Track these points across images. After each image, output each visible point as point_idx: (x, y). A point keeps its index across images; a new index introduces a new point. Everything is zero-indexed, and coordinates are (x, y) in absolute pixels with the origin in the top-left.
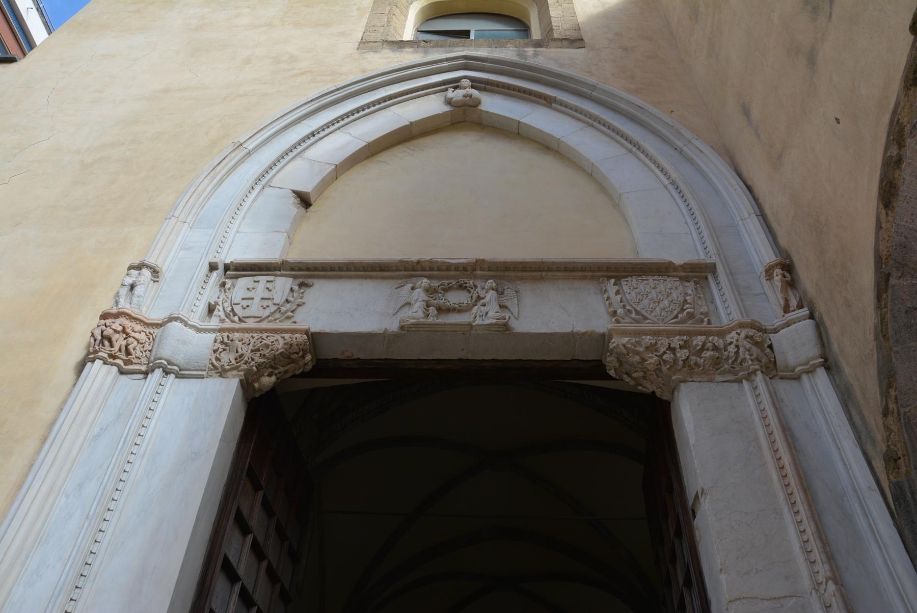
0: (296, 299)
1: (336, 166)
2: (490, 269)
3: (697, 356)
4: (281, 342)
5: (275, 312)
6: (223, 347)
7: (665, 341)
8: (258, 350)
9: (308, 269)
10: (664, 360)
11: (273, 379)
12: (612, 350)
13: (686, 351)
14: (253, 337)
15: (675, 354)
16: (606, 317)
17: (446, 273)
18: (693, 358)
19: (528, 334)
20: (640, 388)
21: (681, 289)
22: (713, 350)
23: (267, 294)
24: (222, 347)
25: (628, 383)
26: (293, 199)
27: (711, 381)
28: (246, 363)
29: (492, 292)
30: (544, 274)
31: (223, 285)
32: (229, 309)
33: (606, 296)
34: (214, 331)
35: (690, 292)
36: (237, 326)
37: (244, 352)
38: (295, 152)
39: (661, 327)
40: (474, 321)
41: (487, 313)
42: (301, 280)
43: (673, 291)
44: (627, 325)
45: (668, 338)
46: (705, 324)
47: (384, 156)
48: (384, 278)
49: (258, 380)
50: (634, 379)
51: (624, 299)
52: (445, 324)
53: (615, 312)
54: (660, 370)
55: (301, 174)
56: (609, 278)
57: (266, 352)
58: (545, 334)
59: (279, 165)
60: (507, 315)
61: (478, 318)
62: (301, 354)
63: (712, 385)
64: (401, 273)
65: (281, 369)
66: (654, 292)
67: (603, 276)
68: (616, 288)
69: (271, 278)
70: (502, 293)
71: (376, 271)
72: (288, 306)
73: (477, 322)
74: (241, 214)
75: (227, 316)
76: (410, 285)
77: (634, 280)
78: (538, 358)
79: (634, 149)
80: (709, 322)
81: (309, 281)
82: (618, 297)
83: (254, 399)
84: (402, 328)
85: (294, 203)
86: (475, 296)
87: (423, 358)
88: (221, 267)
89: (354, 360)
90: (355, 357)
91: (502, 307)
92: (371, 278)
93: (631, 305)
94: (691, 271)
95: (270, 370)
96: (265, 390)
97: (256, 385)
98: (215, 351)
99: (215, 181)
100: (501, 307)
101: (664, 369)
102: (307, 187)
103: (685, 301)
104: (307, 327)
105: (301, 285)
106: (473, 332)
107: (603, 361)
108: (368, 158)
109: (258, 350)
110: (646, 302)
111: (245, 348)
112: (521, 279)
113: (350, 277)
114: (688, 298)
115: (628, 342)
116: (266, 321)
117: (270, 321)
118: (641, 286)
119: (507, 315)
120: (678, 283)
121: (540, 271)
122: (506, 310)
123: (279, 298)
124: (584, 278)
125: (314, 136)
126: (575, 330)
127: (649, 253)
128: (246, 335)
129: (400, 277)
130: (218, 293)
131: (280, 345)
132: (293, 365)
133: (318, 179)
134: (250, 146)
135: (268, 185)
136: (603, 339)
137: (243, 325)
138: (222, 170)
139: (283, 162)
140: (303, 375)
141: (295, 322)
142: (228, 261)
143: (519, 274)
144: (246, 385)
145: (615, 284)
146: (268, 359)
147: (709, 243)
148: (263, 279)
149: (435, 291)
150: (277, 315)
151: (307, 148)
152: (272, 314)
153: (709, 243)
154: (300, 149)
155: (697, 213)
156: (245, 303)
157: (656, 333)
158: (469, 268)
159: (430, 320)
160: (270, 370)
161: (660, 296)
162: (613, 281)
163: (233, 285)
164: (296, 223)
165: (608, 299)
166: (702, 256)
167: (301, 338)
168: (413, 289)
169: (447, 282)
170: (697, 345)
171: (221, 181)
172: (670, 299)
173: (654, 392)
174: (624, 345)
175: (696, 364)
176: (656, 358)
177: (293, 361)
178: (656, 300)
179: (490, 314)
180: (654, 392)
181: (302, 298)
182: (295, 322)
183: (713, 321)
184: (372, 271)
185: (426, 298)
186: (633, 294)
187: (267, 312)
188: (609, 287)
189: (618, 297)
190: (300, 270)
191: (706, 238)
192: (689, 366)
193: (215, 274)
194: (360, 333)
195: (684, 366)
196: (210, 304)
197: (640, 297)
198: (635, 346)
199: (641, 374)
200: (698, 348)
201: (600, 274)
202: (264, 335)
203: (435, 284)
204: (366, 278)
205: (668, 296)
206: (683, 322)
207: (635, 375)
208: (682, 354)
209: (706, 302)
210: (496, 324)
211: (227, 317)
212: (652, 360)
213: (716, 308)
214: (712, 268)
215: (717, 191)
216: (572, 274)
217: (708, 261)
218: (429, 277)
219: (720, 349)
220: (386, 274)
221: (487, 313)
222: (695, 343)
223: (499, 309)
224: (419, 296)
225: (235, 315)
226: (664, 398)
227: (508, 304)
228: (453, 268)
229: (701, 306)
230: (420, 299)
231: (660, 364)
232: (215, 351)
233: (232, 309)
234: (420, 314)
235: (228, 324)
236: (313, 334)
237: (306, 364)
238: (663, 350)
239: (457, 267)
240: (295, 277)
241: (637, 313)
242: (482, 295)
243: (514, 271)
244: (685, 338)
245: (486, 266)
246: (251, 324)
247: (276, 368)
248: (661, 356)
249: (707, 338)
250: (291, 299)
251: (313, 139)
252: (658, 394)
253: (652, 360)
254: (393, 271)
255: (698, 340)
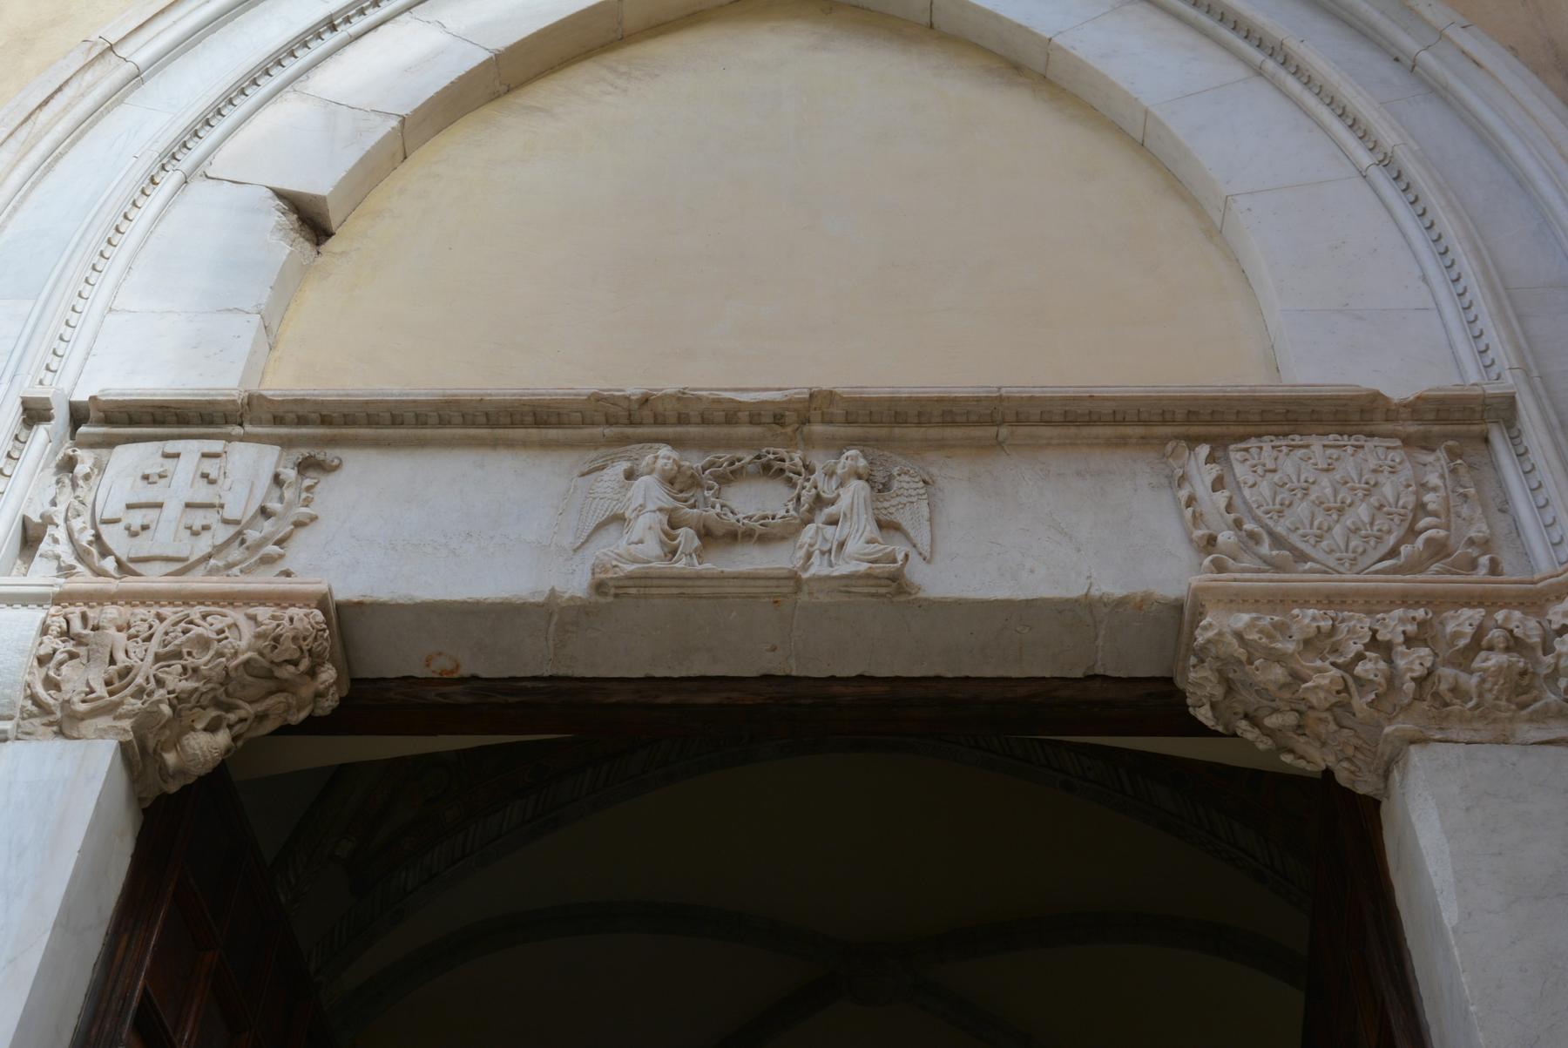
0: (290, 505)
1: (403, 120)
2: (849, 420)
3: (1459, 666)
4: (248, 630)
5: (227, 543)
6: (70, 646)
7: (1358, 625)
8: (177, 655)
9: (325, 421)
10: (1357, 679)
11: (223, 738)
12: (1203, 648)
13: (1424, 651)
14: (161, 619)
15: (1390, 661)
16: (1186, 554)
17: (724, 431)
18: (1447, 673)
19: (959, 603)
20: (1287, 758)
21: (1406, 472)
22: (1507, 649)
23: (203, 493)
24: (63, 647)
25: (1251, 744)
26: (275, 217)
27: (1504, 741)
28: (140, 693)
29: (856, 485)
30: (1004, 431)
31: (69, 464)
32: (86, 537)
33: (1184, 494)
34: (39, 600)
35: (1433, 479)
36: (113, 585)
37: (134, 660)
38: (279, 76)
39: (1349, 581)
40: (805, 567)
41: (842, 545)
42: (305, 452)
43: (1386, 475)
44: (1247, 577)
45: (1369, 613)
46: (1482, 572)
47: (543, 93)
48: (546, 445)
49: (175, 743)
50: (1269, 733)
51: (1237, 501)
52: (722, 577)
53: (1211, 541)
54: (1346, 707)
55: (302, 141)
56: (1194, 441)
57: (201, 660)
58: (1008, 604)
59: (232, 115)
60: (900, 549)
61: (816, 559)
62: (305, 664)
63: (1504, 751)
64: (597, 431)
65: (247, 710)
66: (1325, 480)
67: (1177, 437)
68: (1214, 470)
69: (216, 446)
70: (886, 487)
71: (523, 425)
72: (268, 526)
73: (813, 571)
74: (120, 257)
75: (81, 555)
76: (625, 465)
77: (1267, 447)
78: (989, 672)
79: (1270, 65)
80: (1494, 568)
81: (329, 454)
82: (1221, 498)
83: (164, 797)
84: (599, 587)
85: (279, 228)
86: (807, 496)
87: (660, 673)
88: (61, 415)
89: (462, 680)
90: (465, 671)
91: (886, 526)
92: (510, 444)
93: (1256, 519)
94: (1438, 420)
95: (213, 713)
96: (203, 771)
97: (170, 758)
98: (42, 661)
99: (34, 157)
100: (883, 525)
101: (1360, 703)
102: (317, 181)
103: (1421, 508)
104: (323, 587)
105: (304, 466)
106: (803, 598)
107: (1180, 683)
108: (495, 96)
109: (177, 655)
110: (1302, 509)
111: (136, 649)
112: (941, 445)
113: (450, 444)
114: (1429, 498)
115: (1251, 625)
116: (201, 569)
117: (213, 572)
118: (1288, 465)
119: (900, 549)
120: (1398, 456)
121: (993, 423)
122: (897, 536)
123: (238, 505)
124: (1121, 442)
125: (333, 28)
126: (1095, 592)
127: (1311, 370)
128: (141, 611)
129: (593, 444)
130: (51, 492)
131: (243, 641)
132: (281, 697)
133: (349, 158)
134: (141, 52)
135: (199, 172)
136: (1179, 616)
137: (130, 583)
138: (54, 121)
139: (244, 105)
140: (313, 725)
141: (288, 574)
142: (81, 396)
143: (934, 432)
144: (138, 758)
145: (1211, 459)
146: (208, 680)
147: (1493, 335)
148: (191, 450)
149: (694, 482)
150: (235, 553)
151: (315, 65)
152: (219, 549)
153: (1493, 335)
154: (292, 66)
155: (1459, 250)
156: (137, 519)
157: (1332, 600)
158: (791, 417)
159: (681, 564)
160: (213, 713)
161: (1343, 493)
162: (1204, 450)
163: (100, 467)
164: (288, 286)
165: (1191, 501)
166: (1473, 375)
167: (305, 618)
168: (630, 475)
169: (725, 456)
170: (1457, 635)
171: (53, 158)
172: (1373, 500)
173: (1328, 773)
174: (1239, 635)
175: (1454, 690)
176: (1334, 672)
177: (282, 687)
178: (1332, 504)
179: (850, 547)
180: (1328, 773)
181: (307, 503)
182: (288, 574)
183: (1505, 566)
184: (513, 425)
185: (668, 502)
186: (1265, 488)
187: (204, 545)
188: (1192, 468)
189: (1221, 498)
190: (302, 421)
191: (1486, 322)
192: (1436, 695)
193: (41, 432)
194: (478, 603)
195: (1418, 697)
196: (25, 522)
197: (1284, 495)
198: (1271, 637)
199: (1291, 719)
200: (1462, 643)
201: (1167, 430)
202: (196, 612)
203: (694, 461)
204: (495, 444)
205: (1368, 494)
206: (1414, 566)
207: (1272, 721)
208: (1413, 661)
209: (1484, 506)
210: (867, 576)
211: (80, 558)
212: (1322, 678)
213: (1517, 528)
214: (1504, 411)
215: (1522, 183)
216: (1085, 431)
217: (1492, 389)
218: (677, 443)
219: (1532, 648)
220: (553, 433)
221: (842, 545)
222: (1450, 628)
223: (876, 533)
224: (649, 494)
225: (105, 552)
226: (1361, 789)
227: (903, 518)
228: (743, 416)
229: (1470, 521)
230: (651, 506)
231: (1346, 689)
232: (42, 661)
233: (98, 537)
234: (652, 548)
235: (84, 581)
236: (340, 607)
237: (319, 695)
238: (1353, 649)
239: (731, 414)
240: (286, 443)
241: (1277, 541)
242: (827, 489)
243: (919, 424)
244: (1420, 613)
245: (838, 411)
246: (154, 579)
247: (229, 708)
248: (1348, 667)
249: (1489, 614)
250: (274, 505)
251: (330, 39)
252: (1342, 777)
253: (1322, 678)
254: (572, 425)
255: (1463, 621)
